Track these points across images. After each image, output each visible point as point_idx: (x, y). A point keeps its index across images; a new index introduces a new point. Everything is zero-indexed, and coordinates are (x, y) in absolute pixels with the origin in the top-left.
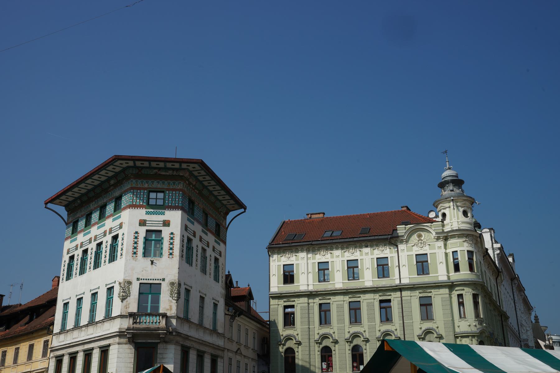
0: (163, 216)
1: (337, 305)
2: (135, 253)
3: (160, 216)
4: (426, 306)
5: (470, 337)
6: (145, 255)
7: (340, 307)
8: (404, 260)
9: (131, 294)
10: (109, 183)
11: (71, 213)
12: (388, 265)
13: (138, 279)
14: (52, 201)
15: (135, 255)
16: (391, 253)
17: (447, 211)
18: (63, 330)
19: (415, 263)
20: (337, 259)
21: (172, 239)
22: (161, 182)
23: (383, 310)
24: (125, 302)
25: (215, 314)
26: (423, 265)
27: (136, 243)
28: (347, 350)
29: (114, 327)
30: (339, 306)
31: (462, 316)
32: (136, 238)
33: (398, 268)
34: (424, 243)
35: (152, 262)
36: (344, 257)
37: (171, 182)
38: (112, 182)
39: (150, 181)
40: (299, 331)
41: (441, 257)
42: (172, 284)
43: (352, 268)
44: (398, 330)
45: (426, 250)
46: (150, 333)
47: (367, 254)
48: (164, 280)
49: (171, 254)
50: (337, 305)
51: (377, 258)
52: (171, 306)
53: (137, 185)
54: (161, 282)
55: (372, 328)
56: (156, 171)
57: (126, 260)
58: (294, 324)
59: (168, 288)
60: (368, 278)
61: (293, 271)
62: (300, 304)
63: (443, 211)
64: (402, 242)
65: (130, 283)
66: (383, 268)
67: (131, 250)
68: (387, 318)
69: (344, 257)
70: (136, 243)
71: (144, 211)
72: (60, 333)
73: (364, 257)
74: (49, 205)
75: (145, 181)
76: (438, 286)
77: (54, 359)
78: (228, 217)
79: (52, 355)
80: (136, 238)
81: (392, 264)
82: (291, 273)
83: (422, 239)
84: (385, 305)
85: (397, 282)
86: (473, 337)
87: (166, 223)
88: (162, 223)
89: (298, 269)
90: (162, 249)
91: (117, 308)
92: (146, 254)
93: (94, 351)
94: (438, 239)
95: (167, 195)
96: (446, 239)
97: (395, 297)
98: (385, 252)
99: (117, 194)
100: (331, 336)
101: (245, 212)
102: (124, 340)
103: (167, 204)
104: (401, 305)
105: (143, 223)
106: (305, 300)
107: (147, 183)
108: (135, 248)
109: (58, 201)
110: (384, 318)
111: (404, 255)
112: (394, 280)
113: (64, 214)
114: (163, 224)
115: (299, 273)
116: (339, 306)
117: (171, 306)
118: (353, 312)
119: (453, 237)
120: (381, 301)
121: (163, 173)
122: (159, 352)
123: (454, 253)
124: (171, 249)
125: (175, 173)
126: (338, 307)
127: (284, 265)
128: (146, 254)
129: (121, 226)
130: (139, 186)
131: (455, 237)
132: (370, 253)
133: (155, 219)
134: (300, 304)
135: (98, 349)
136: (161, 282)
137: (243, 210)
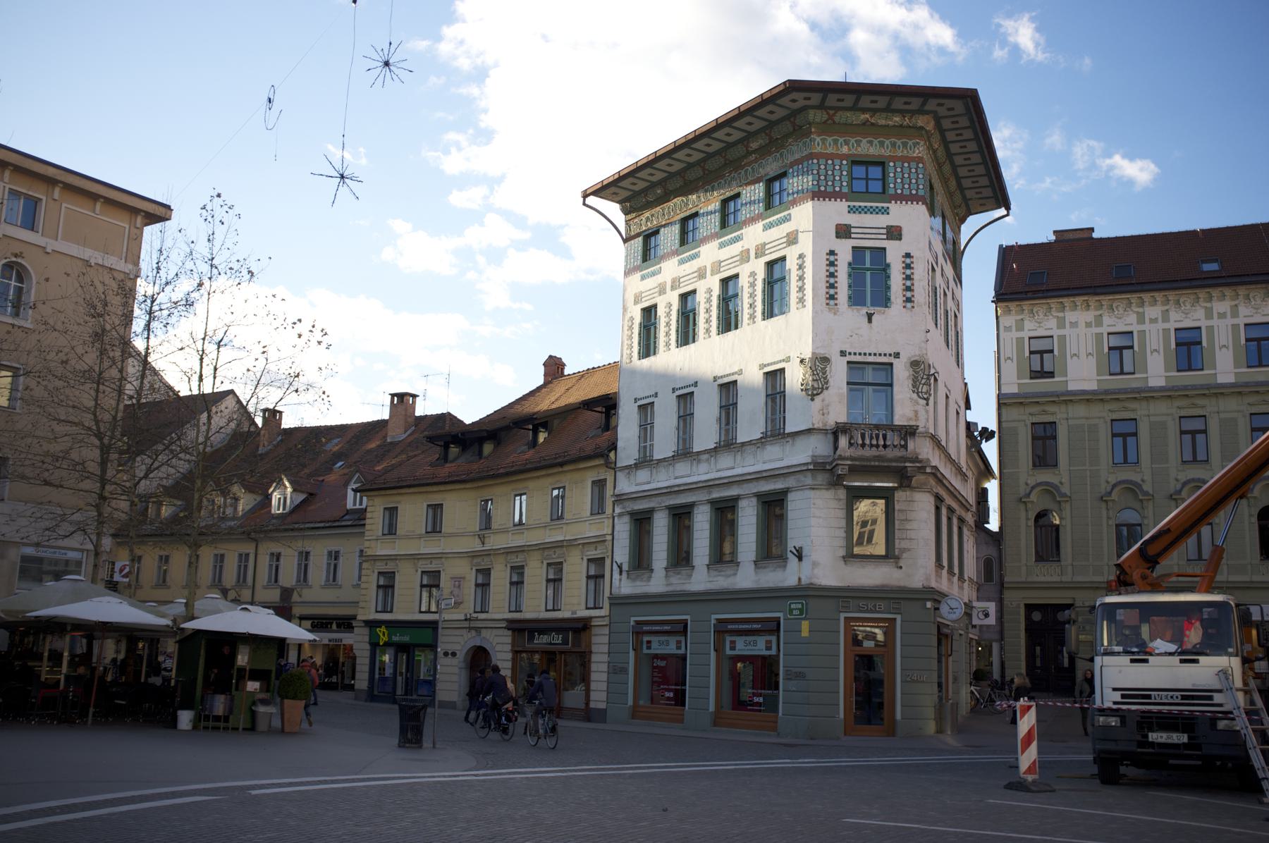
0: (885, 216)
2: (832, 297)
3: (880, 216)
9: (831, 382)
10: (747, 147)
12: (1200, 343)
13: (843, 353)
15: (832, 302)
18: (645, 461)
21: (908, 266)
22: (876, 142)
24: (818, 399)
25: (958, 435)
27: (832, 275)
29: (800, 453)
32: (832, 264)
35: (870, 317)
36: (1022, 329)
37: (899, 142)
38: (754, 145)
39: (853, 141)
47: (1222, 316)
48: (897, 355)
49: (909, 300)
52: (916, 412)
53: (826, 148)
54: (891, 360)
57: (815, 312)
58: (1056, 465)
59: (907, 374)
60: (1157, 371)
65: (825, 360)
69: (1022, 329)
70: (832, 275)
71: (843, 205)
72: (637, 466)
73: (1215, 322)
74: (592, 200)
75: (841, 140)
77: (626, 519)
78: (963, 227)
79: (618, 510)
80: (832, 264)
87: (894, 233)
88: (884, 231)
90: (888, 288)
92: (856, 299)
93: (742, 504)
95: (891, 170)
99: (771, 168)
103: (892, 191)
105: (843, 232)
107: (847, 143)
108: (832, 286)
109: (613, 189)
110: (1188, 456)
113: (619, 217)
114: (887, 234)
117: (916, 412)
122: (897, 507)
124: (908, 289)
128: (856, 299)
129: (792, 239)
130: (830, 150)
132: (1229, 315)
133: (869, 222)
134: (1144, 413)
135: (754, 500)
136: (891, 360)
137: (1003, 211)
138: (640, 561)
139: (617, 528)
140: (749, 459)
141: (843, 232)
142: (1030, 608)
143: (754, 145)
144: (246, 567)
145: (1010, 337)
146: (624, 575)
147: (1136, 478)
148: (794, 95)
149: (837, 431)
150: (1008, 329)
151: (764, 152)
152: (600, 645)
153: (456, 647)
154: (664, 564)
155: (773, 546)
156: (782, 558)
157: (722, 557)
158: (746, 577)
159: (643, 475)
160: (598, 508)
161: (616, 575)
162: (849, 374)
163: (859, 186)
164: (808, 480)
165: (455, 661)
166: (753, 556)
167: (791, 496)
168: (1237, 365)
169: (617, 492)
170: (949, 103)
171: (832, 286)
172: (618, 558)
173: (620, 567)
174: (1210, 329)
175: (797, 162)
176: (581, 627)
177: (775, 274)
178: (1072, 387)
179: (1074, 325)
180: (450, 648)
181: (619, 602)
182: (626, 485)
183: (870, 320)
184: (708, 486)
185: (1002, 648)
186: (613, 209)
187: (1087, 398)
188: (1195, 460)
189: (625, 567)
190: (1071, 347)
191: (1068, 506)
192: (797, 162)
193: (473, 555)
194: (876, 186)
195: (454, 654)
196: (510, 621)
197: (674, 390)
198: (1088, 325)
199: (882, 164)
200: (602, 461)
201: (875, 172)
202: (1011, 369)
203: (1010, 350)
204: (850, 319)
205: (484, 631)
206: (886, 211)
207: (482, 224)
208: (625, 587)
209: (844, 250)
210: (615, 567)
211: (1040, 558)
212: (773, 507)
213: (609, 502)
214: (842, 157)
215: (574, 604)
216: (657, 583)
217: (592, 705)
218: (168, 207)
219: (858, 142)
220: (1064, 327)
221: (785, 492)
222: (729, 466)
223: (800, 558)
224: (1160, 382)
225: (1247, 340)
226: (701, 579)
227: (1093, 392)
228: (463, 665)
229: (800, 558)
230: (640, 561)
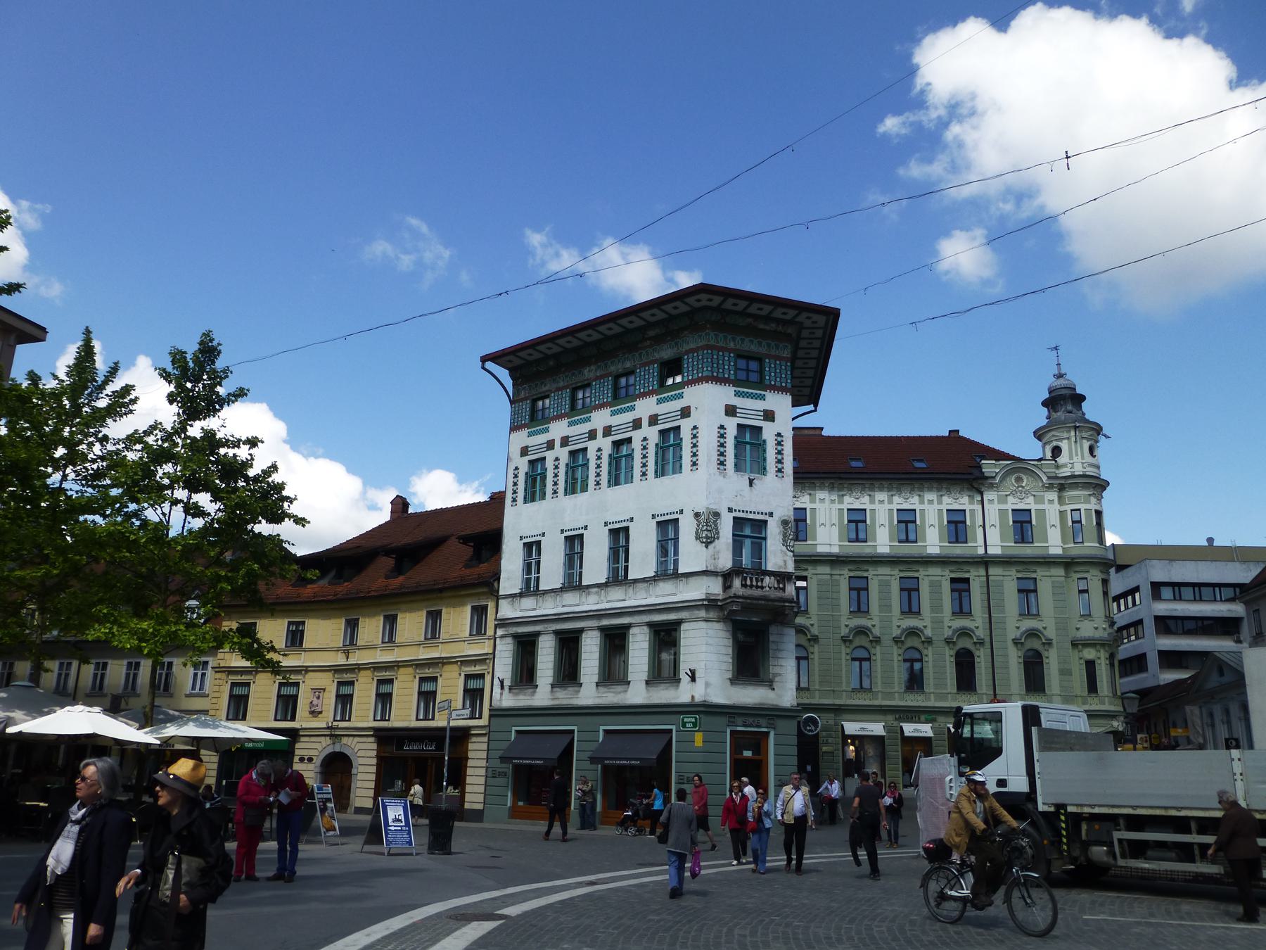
1: (819, 581)
4: (910, 591)
6: (738, 468)
9: (721, 534)
11: (521, 384)
13: (730, 510)
14: (496, 358)
17: (1064, 445)
20: (882, 507)
24: (711, 547)
28: (947, 658)
29: (695, 591)
32: (722, 436)
35: (751, 482)
38: (651, 333)
40: (876, 621)
41: (1052, 516)
42: (785, 523)
43: (907, 523)
45: (1029, 503)
46: (749, 605)
47: (881, 502)
48: (771, 514)
50: (819, 581)
54: (767, 518)
55: (938, 623)
56: (750, 320)
60: (933, 542)
63: (1055, 443)
64: (991, 486)
66: (957, 526)
67: (715, 457)
73: (926, 506)
74: (489, 365)
76: (1048, 562)
80: (722, 436)
84: (960, 586)
85: (981, 551)
86: (1103, 645)
89: (873, 519)
90: (765, 459)
91: (691, 556)
94: (1050, 487)
96: (1062, 488)
97: (976, 577)
98: (1027, 501)
99: (667, 353)
100: (870, 630)
102: (712, 615)
104: (985, 590)
106: (825, 569)
107: (734, 340)
113: (508, 383)
116: (883, 583)
119: (1075, 486)
120: (953, 580)
121: (762, 326)
122: (771, 639)
125: (780, 328)
126: (932, 584)
129: (685, 412)
130: (721, 344)
133: (751, 406)
134: (876, 576)
135: (646, 629)
136: (767, 518)
137: (811, 407)
138: (525, 675)
139: (498, 648)
140: (642, 594)
141: (731, 411)
143: (651, 333)
144: (67, 675)
146: (506, 689)
147: (869, 623)
148: (703, 296)
149: (727, 577)
151: (659, 340)
152: (477, 752)
153: (312, 753)
154: (550, 680)
155: (664, 669)
156: (674, 679)
157: (612, 673)
158: (637, 693)
159: (528, 603)
160: (478, 627)
161: (497, 689)
162: (734, 529)
163: (742, 375)
164: (702, 613)
165: (311, 766)
166: (645, 676)
167: (684, 626)
168: (941, 541)
169: (499, 616)
170: (815, 317)
171: (722, 454)
172: (499, 673)
173: (502, 682)
174: (813, 510)
175: (692, 351)
176: (461, 736)
177: (670, 439)
178: (820, 549)
179: (822, 500)
180: (306, 753)
181: (496, 713)
182: (507, 610)
183: (751, 485)
184: (599, 615)
186: (504, 374)
188: (910, 611)
189: (507, 683)
190: (821, 518)
191: (816, 649)
192: (692, 351)
193: (337, 670)
194: (754, 377)
195: (310, 760)
196: (376, 730)
197: (562, 531)
198: (833, 501)
199: (760, 360)
200: (485, 590)
201: (754, 365)
204: (735, 482)
205: (345, 740)
206: (763, 398)
207: (1045, 404)
208: (507, 700)
209: (731, 425)
210: (496, 682)
212: (666, 637)
213: (491, 623)
214: (730, 350)
215: (451, 713)
216: (543, 695)
217: (467, 806)
218: (43, 330)
219: (743, 340)
221: (678, 623)
222: (617, 598)
223: (693, 679)
224: (1059, 551)
225: (849, 521)
226: (588, 693)
227: (837, 556)
228: (318, 770)
229: (693, 679)
230: (525, 675)
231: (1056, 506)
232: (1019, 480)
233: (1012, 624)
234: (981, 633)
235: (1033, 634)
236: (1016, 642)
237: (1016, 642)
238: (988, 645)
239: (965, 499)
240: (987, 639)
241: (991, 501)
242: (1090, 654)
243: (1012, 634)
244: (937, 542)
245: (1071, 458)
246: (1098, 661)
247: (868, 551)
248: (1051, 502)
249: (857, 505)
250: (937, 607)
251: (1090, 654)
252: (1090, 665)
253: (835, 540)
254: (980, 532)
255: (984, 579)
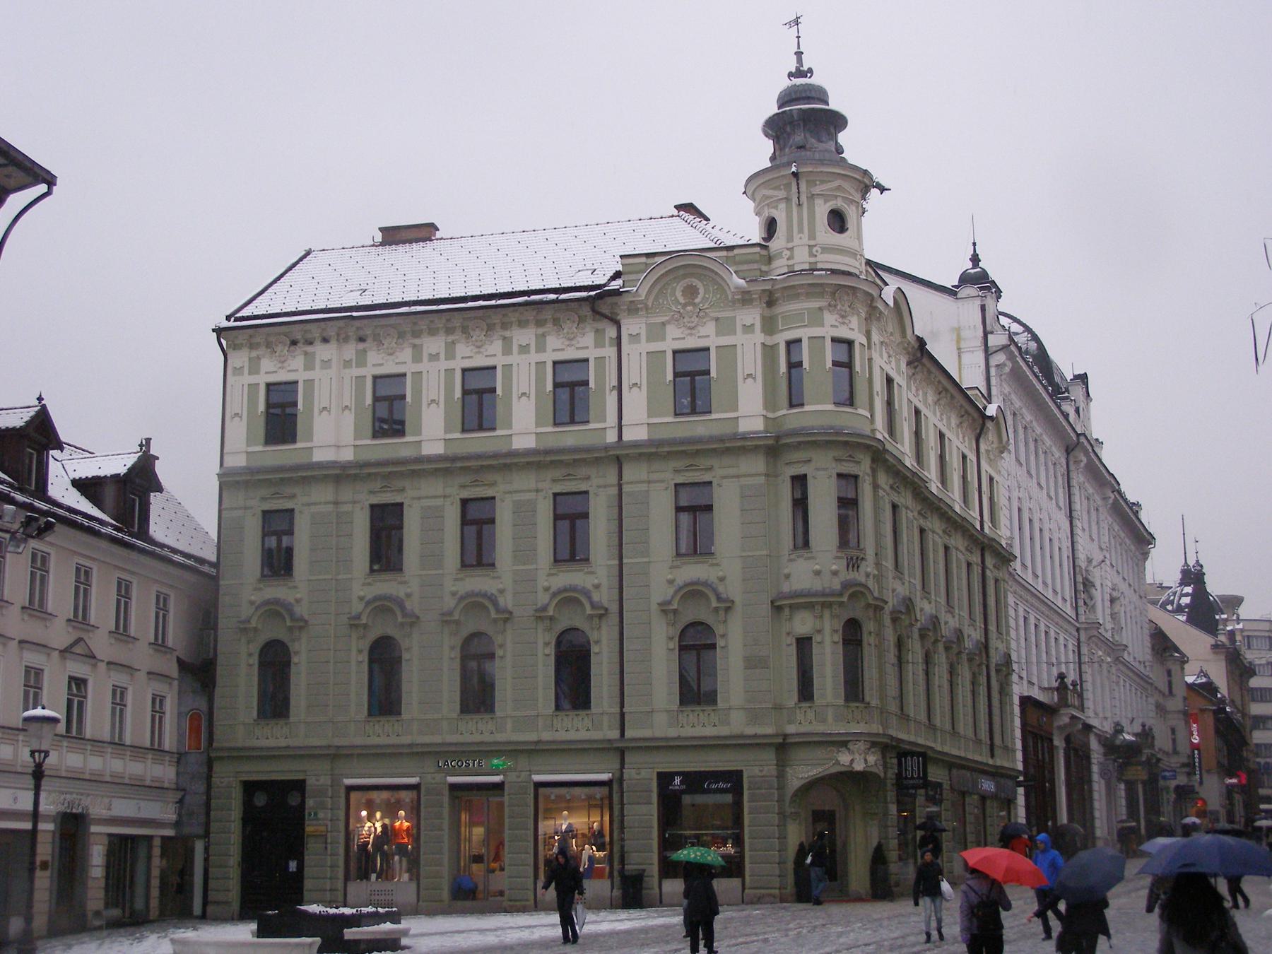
4: (695, 509)
5: (818, 608)
7: (524, 512)
8: (635, 369)
12: (708, 372)
16: (599, 344)
19: (670, 377)
23: (472, 530)
26: (693, 382)
30: (431, 519)
31: (803, 542)
33: (615, 393)
34: (701, 313)
41: (749, 358)
44: (604, 589)
45: (707, 335)
47: (748, 329)
51: (555, 363)
60: (433, 431)
61: (295, 404)
62: (310, 507)
64: (633, 310)
68: (571, 549)
73: (514, 359)
76: (733, 446)
81: (599, 379)
82: (288, 411)
83: (697, 301)
89: (417, 392)
96: (771, 300)
98: (703, 331)
101: (48, 194)
104: (616, 510)
111: (635, 356)
112: (602, 428)
115: (312, 410)
118: (564, 525)
123: (793, 344)
126: (518, 508)
127: (269, 386)
131: (797, 296)
132: (442, 356)
137: (43, 188)
142: (250, 788)
145: (239, 383)
150: (238, 371)
168: (249, 442)
174: (309, 383)
178: (318, 456)
179: (326, 364)
185: (207, 849)
187: (340, 475)
190: (322, 396)
198: (347, 364)
202: (238, 431)
203: (238, 402)
211: (466, 708)
220: (313, 369)
224: (757, 425)
225: (556, 385)
227: (344, 466)
231: (759, 337)
232: (691, 292)
233: (661, 571)
234: (605, 596)
235: (693, 592)
236: (665, 608)
237: (665, 608)
238: (615, 619)
239: (588, 339)
240: (614, 608)
241: (635, 338)
242: (803, 624)
243: (660, 591)
244: (532, 427)
245: (790, 238)
246: (817, 638)
247: (406, 453)
248: (748, 329)
249: (390, 368)
250: (524, 553)
251: (803, 624)
252: (804, 644)
253: (348, 436)
254: (611, 400)
255: (615, 491)
